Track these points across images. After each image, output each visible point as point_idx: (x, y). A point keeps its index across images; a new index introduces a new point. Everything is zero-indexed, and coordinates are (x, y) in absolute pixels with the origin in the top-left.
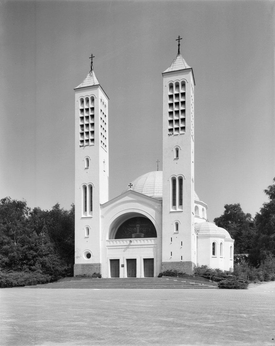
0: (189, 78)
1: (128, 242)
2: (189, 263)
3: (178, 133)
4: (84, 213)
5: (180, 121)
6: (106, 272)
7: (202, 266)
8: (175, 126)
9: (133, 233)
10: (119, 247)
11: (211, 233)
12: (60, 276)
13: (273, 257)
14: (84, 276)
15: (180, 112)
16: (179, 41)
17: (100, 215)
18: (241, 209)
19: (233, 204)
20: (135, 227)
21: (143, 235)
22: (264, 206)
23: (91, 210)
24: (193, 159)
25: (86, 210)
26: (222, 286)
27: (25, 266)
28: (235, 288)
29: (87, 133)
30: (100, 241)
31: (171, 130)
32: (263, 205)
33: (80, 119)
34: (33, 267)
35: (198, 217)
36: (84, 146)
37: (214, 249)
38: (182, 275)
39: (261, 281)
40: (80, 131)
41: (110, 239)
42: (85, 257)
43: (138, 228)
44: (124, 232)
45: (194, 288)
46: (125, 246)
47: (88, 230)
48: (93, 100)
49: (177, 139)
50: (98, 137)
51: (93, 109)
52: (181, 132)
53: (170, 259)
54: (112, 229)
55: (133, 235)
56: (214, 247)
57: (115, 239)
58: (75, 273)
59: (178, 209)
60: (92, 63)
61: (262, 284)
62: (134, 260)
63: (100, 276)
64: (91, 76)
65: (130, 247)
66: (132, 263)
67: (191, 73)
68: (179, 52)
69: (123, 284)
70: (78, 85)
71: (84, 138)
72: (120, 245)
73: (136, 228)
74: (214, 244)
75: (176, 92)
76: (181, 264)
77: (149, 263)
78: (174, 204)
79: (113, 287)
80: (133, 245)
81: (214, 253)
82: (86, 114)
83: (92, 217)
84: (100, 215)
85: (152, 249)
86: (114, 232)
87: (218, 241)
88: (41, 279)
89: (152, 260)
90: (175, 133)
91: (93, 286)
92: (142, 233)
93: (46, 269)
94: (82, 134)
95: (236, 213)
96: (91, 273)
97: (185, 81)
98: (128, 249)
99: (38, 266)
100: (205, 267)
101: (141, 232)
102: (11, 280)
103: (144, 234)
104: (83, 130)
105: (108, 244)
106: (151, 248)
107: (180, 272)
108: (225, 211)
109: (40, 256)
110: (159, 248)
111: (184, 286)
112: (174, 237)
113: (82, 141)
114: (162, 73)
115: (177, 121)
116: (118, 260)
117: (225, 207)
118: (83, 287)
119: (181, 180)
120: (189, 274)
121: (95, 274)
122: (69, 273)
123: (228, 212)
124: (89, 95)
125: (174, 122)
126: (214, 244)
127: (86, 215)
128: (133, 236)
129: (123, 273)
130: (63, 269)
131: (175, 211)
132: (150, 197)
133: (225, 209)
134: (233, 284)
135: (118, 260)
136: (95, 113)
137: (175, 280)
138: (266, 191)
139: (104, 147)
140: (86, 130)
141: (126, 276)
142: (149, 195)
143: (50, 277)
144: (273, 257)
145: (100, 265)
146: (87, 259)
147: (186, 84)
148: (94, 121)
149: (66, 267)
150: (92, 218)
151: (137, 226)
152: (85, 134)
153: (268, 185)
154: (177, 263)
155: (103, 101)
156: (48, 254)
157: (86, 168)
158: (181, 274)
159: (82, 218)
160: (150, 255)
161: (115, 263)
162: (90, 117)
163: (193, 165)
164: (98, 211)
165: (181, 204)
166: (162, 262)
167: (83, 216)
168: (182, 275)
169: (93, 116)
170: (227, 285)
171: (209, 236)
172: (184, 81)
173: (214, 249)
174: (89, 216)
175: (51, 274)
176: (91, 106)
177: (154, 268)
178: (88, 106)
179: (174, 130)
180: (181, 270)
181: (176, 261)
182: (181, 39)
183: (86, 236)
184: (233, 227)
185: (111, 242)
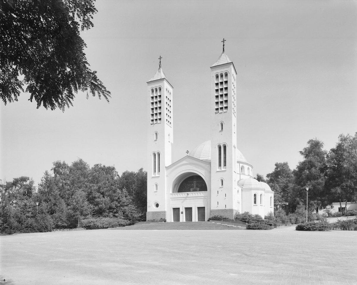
1: (186, 195)
2: (231, 211)
3: (222, 112)
4: (154, 174)
5: (224, 102)
6: (170, 218)
7: (245, 212)
8: (220, 106)
10: (179, 199)
11: (253, 187)
12: (137, 221)
13: (303, 204)
14: (153, 221)
15: (224, 96)
16: (224, 42)
17: (166, 175)
18: (288, 167)
19: (282, 163)
20: (193, 183)
21: (198, 189)
22: (300, 164)
25: (220, 165)
26: (249, 228)
27: (111, 214)
28: (258, 229)
29: (156, 114)
30: (166, 194)
31: (217, 109)
32: (299, 164)
33: (151, 104)
34: (117, 215)
35: (244, 174)
36: (154, 123)
37: (255, 199)
38: (225, 220)
39: (292, 224)
40: (151, 113)
41: (173, 192)
42: (154, 207)
43: (195, 184)
44: (185, 187)
45: (228, 229)
46: (184, 197)
47: (157, 186)
48: (160, 89)
50: (164, 117)
51: (160, 96)
52: (224, 110)
54: (175, 186)
55: (191, 189)
56: (256, 198)
58: (147, 219)
60: (160, 62)
61: (292, 226)
62: (190, 209)
63: (165, 221)
64: (160, 72)
65: (187, 198)
66: (189, 210)
67: (232, 66)
68: (224, 50)
69: (183, 227)
70: (213, 64)
71: (154, 118)
72: (180, 197)
73: (194, 184)
74: (255, 195)
75: (220, 81)
76: (226, 211)
77: (201, 210)
78: (220, 165)
80: (190, 197)
81: (255, 202)
82: (155, 100)
84: (166, 175)
85: (202, 200)
86: (177, 187)
87: (258, 193)
88: (122, 223)
89: (203, 208)
90: (220, 111)
93: (126, 217)
94: (153, 115)
95: (284, 170)
96: (159, 218)
97: (227, 72)
98: (186, 200)
99: (120, 213)
100: (248, 213)
101: (197, 187)
102: (98, 224)
104: (153, 112)
105: (172, 196)
106: (201, 199)
107: (224, 217)
108: (276, 168)
109: (122, 206)
110: (208, 199)
111: (221, 228)
112: (220, 190)
115: (222, 102)
116: (179, 208)
117: (276, 165)
119: (225, 147)
120: (231, 218)
121: (161, 219)
122: (143, 219)
123: (278, 169)
125: (219, 103)
126: (255, 195)
127: (155, 175)
128: (191, 190)
129: (183, 218)
130: (139, 215)
131: (221, 170)
132: (202, 160)
133: (275, 167)
134: (258, 226)
135: (179, 208)
136: (162, 99)
137: (218, 223)
138: (301, 152)
139: (169, 124)
140: (155, 112)
141: (185, 221)
142: (201, 159)
143: (129, 222)
144: (303, 204)
145: (165, 212)
146: (154, 207)
149: (140, 215)
152: (154, 115)
153: (303, 148)
154: (222, 211)
155: (168, 90)
156: (128, 205)
157: (155, 140)
158: (225, 219)
159: (152, 177)
161: (176, 211)
162: (158, 102)
164: (164, 172)
165: (225, 165)
166: (211, 209)
167: (153, 176)
168: (225, 220)
169: (160, 102)
170: (253, 226)
171: (251, 189)
173: (255, 199)
174: (157, 175)
175: (130, 220)
176: (225, 80)
177: (205, 214)
178: (157, 94)
179: (219, 109)
180: (225, 215)
181: (222, 209)
183: (155, 191)
184: (282, 181)
185: (174, 196)
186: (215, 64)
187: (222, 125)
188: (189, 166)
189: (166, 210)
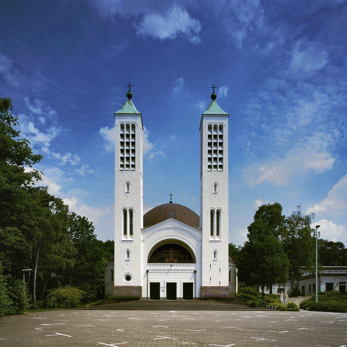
0: (138, 122)
3: (123, 169)
6: (146, 293)
9: (166, 259)
16: (214, 89)
21: (176, 260)
23: (131, 233)
24: (142, 195)
43: (171, 254)
49: (127, 175)
53: (209, 284)
55: (167, 260)
57: (149, 263)
59: (129, 238)
66: (171, 287)
70: (117, 111)
73: (170, 254)
77: (188, 287)
78: (125, 233)
79: (174, 307)
83: (221, 241)
89: (191, 284)
91: (186, 308)
92: (176, 259)
98: (169, 274)
101: (175, 257)
103: (177, 260)
112: (213, 264)
113: (122, 166)
114: (114, 113)
118: (206, 309)
119: (218, 213)
124: (125, 122)
127: (127, 238)
129: (163, 294)
131: (214, 240)
147: (136, 127)
148: (223, 148)
150: (221, 242)
151: (171, 252)
157: (126, 192)
159: (122, 241)
160: (188, 279)
161: (155, 287)
163: (142, 199)
165: (131, 233)
166: (202, 286)
172: (128, 124)
182: (212, 88)
186: (120, 110)
187: (128, 186)
188: (172, 230)
189: (142, 285)
